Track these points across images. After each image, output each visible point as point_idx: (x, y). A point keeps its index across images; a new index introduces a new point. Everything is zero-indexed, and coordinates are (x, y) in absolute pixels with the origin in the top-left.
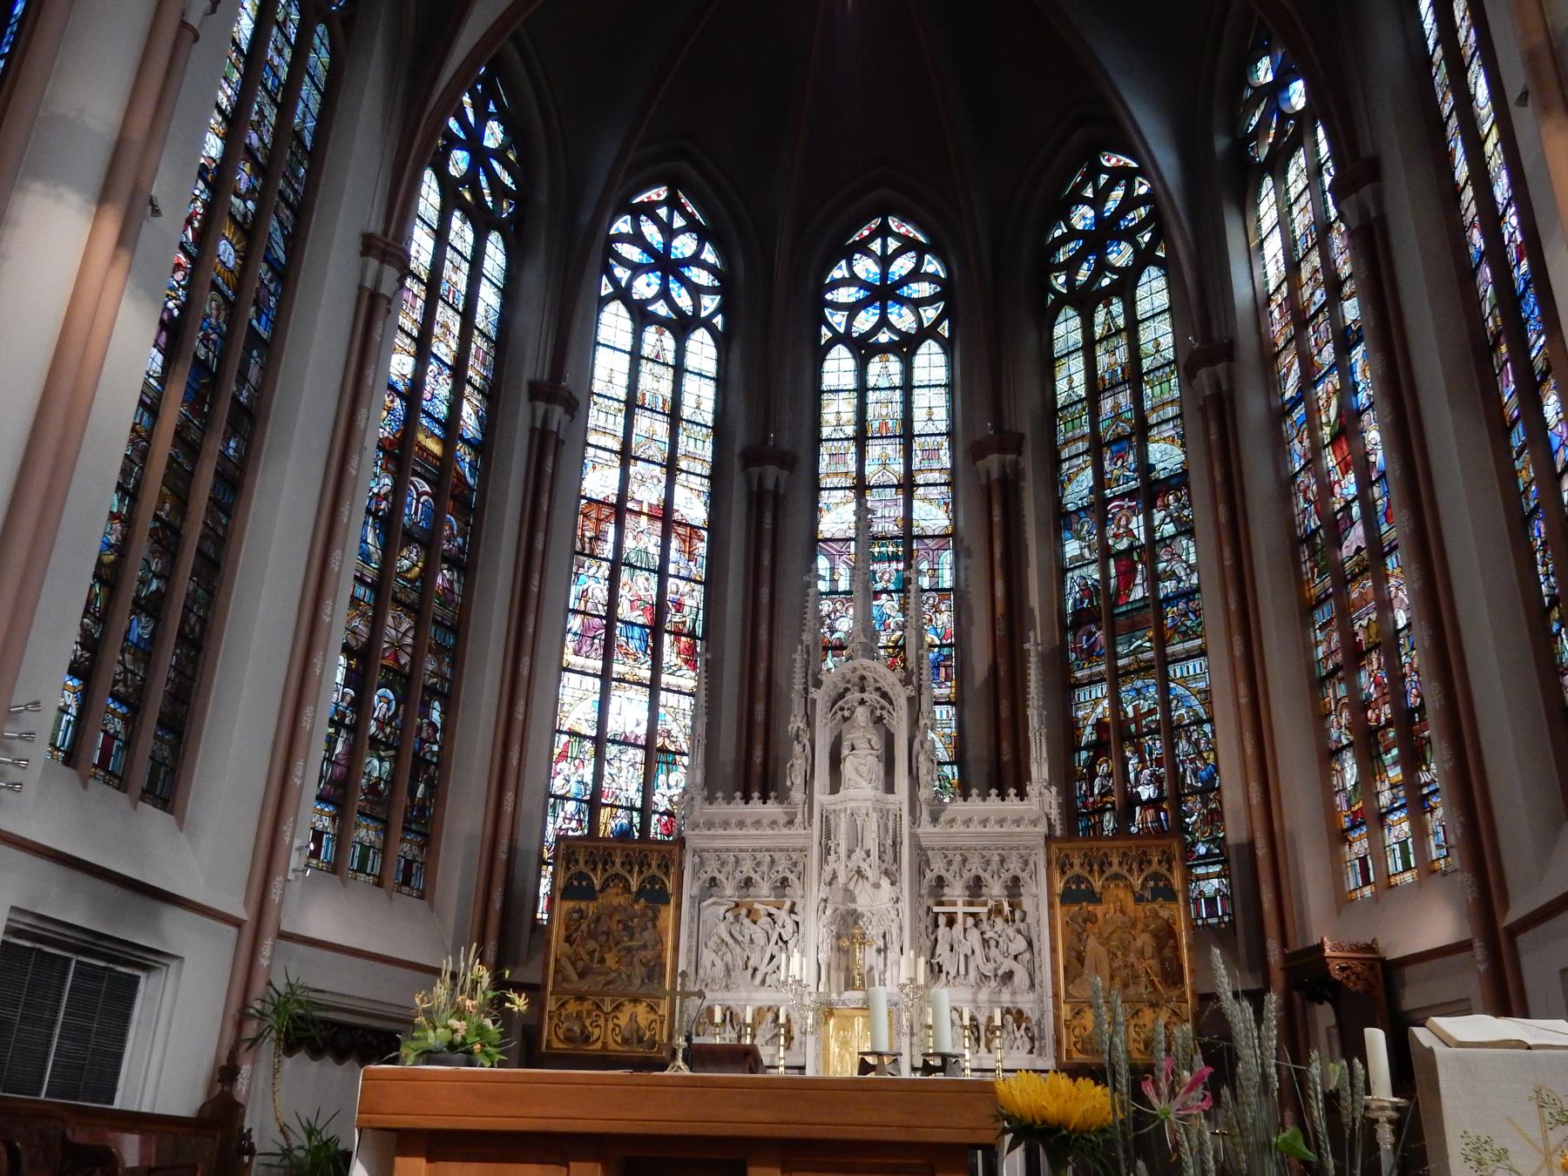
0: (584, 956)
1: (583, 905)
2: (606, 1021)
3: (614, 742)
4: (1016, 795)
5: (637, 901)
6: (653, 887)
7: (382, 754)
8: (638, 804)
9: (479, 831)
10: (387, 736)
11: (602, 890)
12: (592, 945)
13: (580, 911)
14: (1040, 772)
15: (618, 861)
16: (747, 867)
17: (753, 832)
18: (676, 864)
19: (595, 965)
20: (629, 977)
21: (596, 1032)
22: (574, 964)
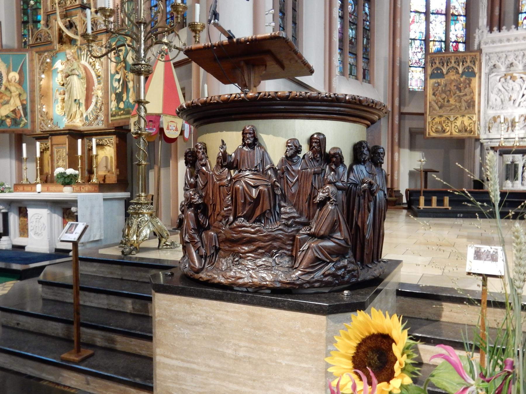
0: (442, 101)
1: (439, 80)
2: (451, 124)
3: (433, 13)
4: (506, 29)
5: (462, 77)
6: (468, 71)
7: (352, 27)
8: (444, 40)
9: (388, 56)
10: (353, 20)
11: (447, 73)
12: (444, 95)
13: (438, 83)
14: (483, 22)
15: (453, 61)
16: (511, 59)
17: (515, 43)
18: (478, 60)
19: (446, 103)
20: (460, 107)
21: (448, 128)
22: (437, 103)
